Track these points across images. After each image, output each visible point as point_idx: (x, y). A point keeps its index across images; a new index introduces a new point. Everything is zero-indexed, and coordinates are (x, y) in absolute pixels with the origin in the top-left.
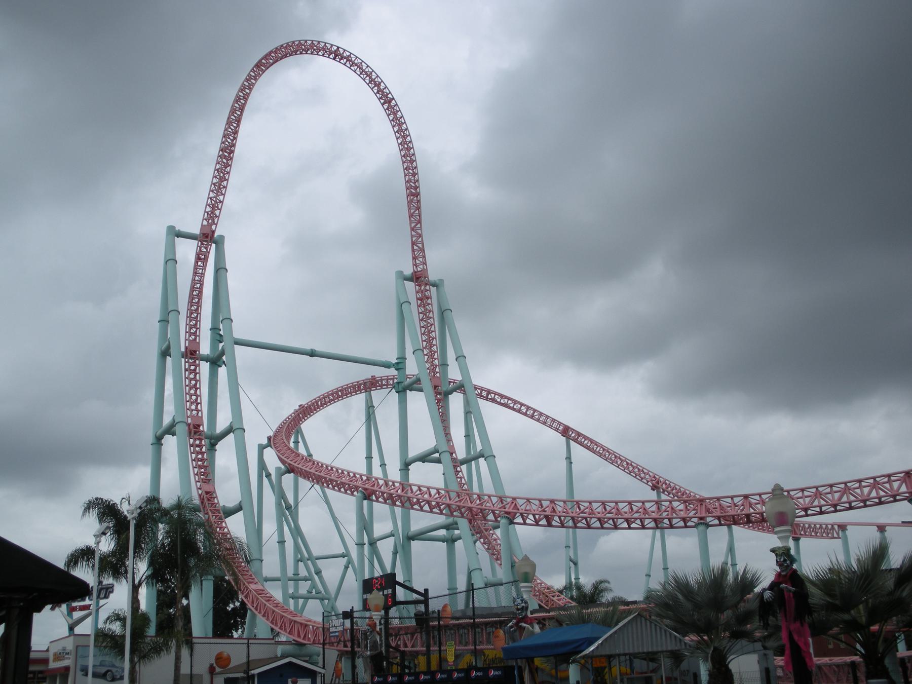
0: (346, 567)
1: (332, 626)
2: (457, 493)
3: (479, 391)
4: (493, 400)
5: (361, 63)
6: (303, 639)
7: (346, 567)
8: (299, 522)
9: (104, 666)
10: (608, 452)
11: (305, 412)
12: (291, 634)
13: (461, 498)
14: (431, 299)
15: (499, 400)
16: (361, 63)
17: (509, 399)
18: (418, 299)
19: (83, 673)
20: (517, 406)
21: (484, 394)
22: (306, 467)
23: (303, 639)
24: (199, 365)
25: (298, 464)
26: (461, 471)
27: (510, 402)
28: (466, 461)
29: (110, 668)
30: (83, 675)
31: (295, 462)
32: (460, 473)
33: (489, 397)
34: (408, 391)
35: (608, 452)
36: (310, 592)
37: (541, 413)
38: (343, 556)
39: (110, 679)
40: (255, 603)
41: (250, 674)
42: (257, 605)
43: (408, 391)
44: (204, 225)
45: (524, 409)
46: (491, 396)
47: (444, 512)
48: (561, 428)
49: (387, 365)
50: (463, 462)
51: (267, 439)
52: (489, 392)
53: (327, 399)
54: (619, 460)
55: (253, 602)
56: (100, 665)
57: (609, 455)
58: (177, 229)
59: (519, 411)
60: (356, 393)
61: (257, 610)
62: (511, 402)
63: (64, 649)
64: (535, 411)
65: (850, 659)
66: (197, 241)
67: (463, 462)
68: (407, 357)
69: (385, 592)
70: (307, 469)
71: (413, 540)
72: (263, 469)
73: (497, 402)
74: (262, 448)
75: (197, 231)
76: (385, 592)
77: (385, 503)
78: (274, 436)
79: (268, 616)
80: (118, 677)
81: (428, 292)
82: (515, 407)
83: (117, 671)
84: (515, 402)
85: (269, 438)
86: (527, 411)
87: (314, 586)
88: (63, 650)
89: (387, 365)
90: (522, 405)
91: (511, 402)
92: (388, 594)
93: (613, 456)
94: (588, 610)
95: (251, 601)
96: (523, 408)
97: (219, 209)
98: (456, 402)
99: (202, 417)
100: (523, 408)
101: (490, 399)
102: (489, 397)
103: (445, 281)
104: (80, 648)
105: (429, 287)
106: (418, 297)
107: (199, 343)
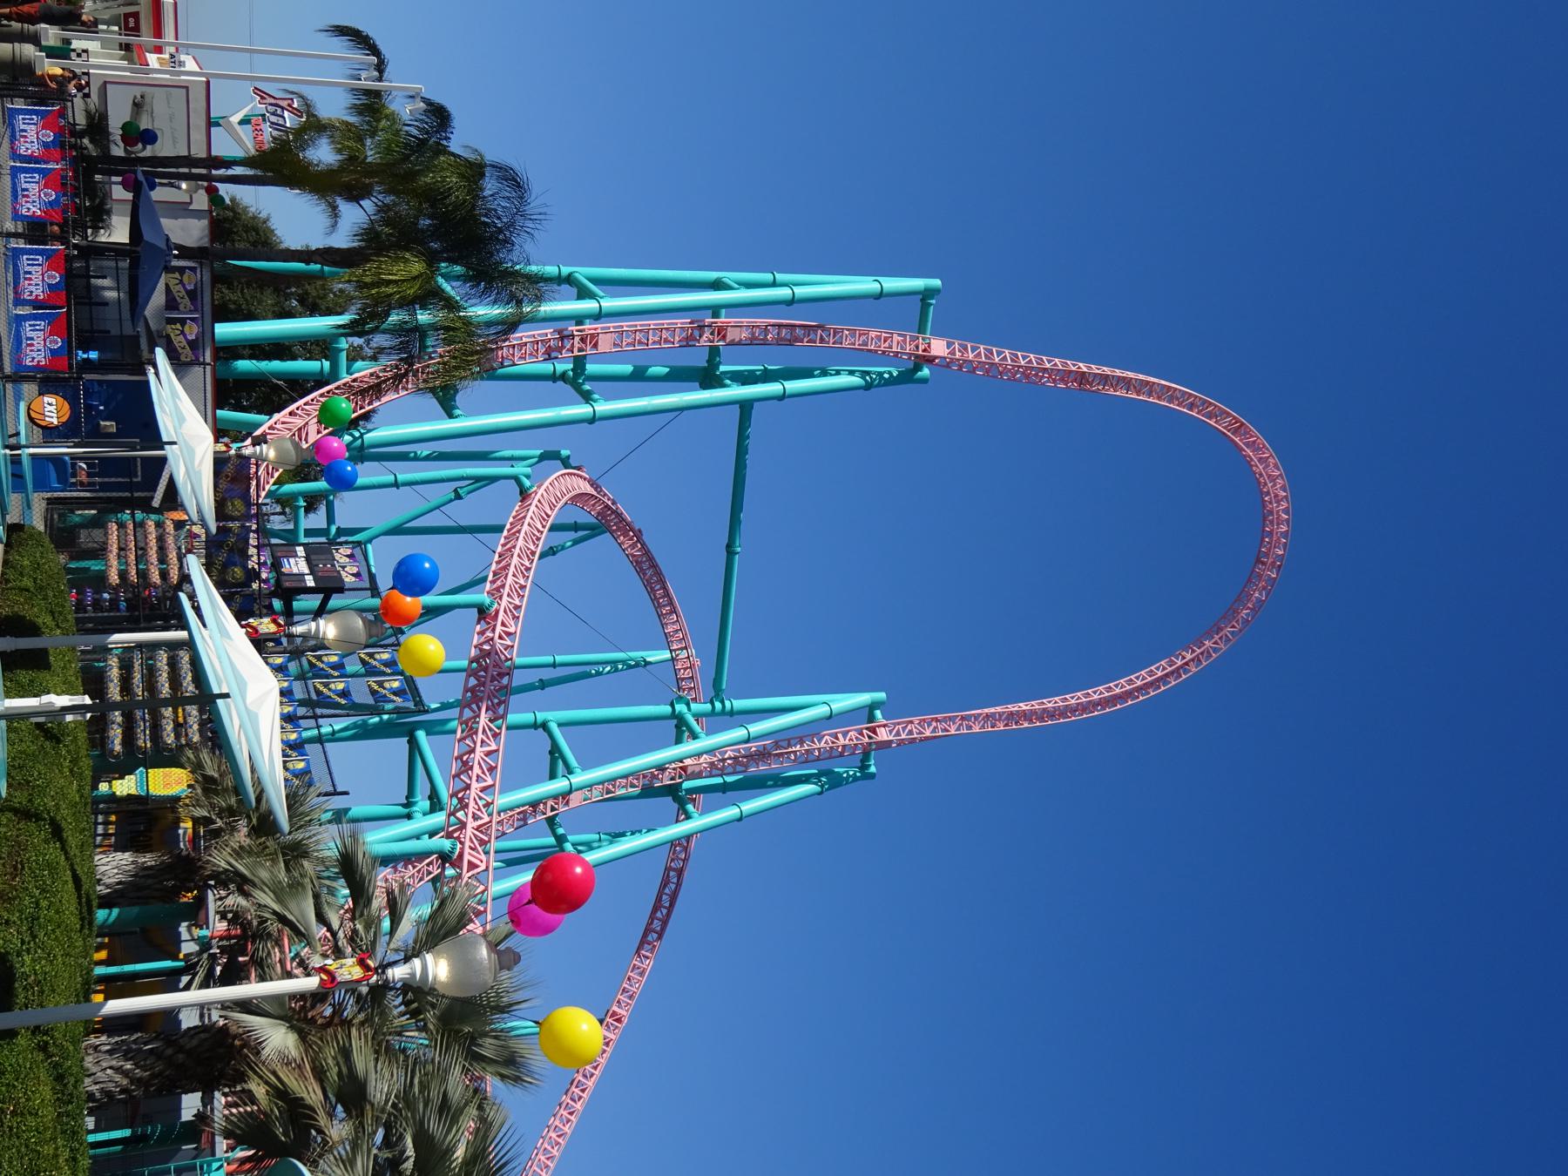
2: (492, 803)
13: (484, 810)
15: (673, 886)
22: (532, 518)
25: (529, 525)
27: (665, 911)
30: (135, 97)
31: (539, 501)
33: (672, 874)
40: (283, 426)
41: (146, 366)
42: (278, 430)
46: (657, 925)
47: (452, 818)
53: (649, 573)
55: (283, 423)
61: (269, 428)
62: (664, 914)
70: (528, 520)
71: (409, 742)
73: (664, 888)
77: (466, 690)
84: (665, 923)
88: (180, 62)
91: (664, 914)
92: (304, 581)
94: (81, 399)
100: (655, 936)
101: (668, 875)
102: (672, 874)
104: (184, 90)
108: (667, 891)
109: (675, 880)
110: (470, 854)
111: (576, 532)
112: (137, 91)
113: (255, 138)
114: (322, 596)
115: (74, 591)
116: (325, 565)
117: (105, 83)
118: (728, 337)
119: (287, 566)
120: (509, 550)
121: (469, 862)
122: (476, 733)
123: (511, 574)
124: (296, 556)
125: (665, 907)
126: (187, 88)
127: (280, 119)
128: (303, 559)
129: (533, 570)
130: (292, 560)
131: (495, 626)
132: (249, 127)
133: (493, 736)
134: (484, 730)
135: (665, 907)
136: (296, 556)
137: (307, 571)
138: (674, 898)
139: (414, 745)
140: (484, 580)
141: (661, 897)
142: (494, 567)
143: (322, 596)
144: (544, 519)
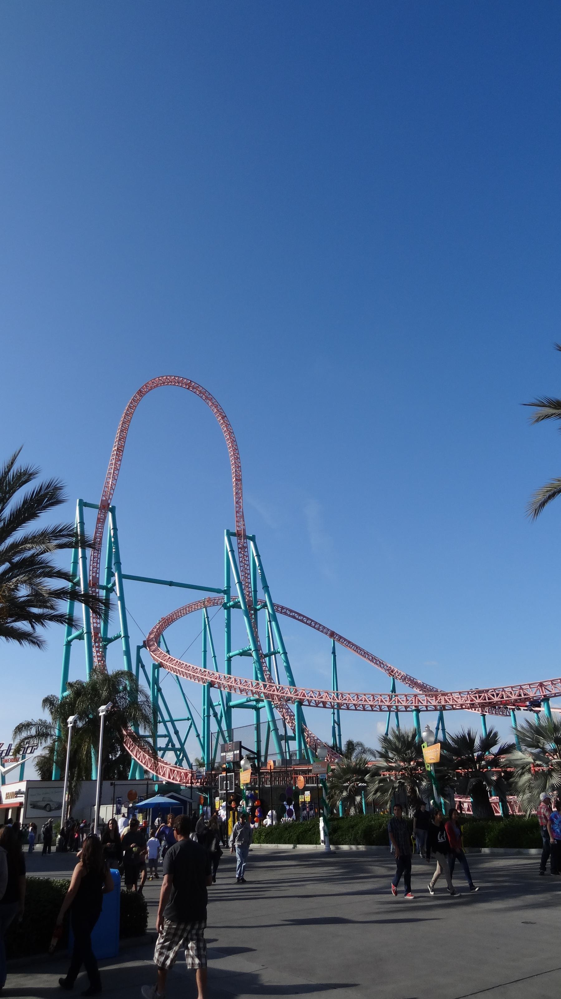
0: (190, 727)
1: (198, 772)
3: (276, 607)
4: (285, 614)
5: (205, 392)
6: (172, 780)
7: (190, 727)
8: (261, 739)
9: (45, 801)
10: (367, 654)
11: (167, 622)
12: (164, 776)
14: (247, 548)
16: (205, 392)
17: (304, 616)
18: (239, 548)
19: (31, 806)
20: (309, 622)
21: (280, 609)
23: (172, 780)
24: (98, 593)
26: (265, 662)
27: (304, 619)
28: (269, 655)
29: (49, 803)
30: (32, 808)
32: (265, 664)
33: (283, 611)
34: (231, 608)
35: (367, 654)
36: (167, 745)
37: (324, 626)
38: (188, 719)
39: (48, 810)
42: (140, 757)
43: (231, 608)
44: (103, 500)
45: (288, 612)
46: (309, 622)
48: (329, 632)
49: (218, 591)
50: (266, 656)
51: (143, 643)
52: (283, 608)
54: (367, 655)
55: (136, 755)
56: (43, 801)
57: (360, 652)
58: (84, 501)
59: (310, 625)
60: (98, 563)
63: (20, 790)
64: (320, 625)
65: (552, 802)
66: (98, 510)
67: (266, 656)
68: (231, 586)
69: (235, 752)
71: (233, 708)
72: (140, 662)
73: (288, 614)
74: (139, 648)
75: (99, 503)
76: (235, 752)
78: (148, 640)
79: (147, 764)
80: (54, 808)
81: (246, 544)
82: (308, 622)
83: (53, 804)
84: (308, 619)
85: (144, 642)
86: (311, 623)
87: (170, 741)
89: (218, 591)
90: (312, 621)
92: (236, 754)
93: (363, 652)
95: (135, 754)
96: (313, 623)
97: (521, 687)
98: (264, 615)
99: (100, 628)
103: (256, 536)
104: (29, 789)
105: (246, 540)
106: (239, 547)
107: (98, 578)
108: (297, 617)
109: (294, 614)
110: (300, 696)
111: (397, 730)
112: (29, 806)
113: (12, 762)
114: (242, 749)
115: (252, 826)
116: (230, 747)
117: (25, 818)
118: (433, 731)
119: (230, 759)
120: (173, 669)
121: (302, 696)
122: (245, 689)
123: (188, 672)
124: (226, 756)
125: (303, 618)
126: (28, 788)
127: (4, 752)
128: (227, 754)
129: (194, 666)
130: (227, 757)
131: (197, 676)
132: (6, 764)
133: (258, 685)
134: (244, 686)
135: (303, 618)
136: (226, 756)
137: (233, 753)
138: (300, 615)
139: (234, 706)
140: (177, 676)
141: (291, 616)
142: (172, 672)
143: (242, 749)
144: (160, 653)
